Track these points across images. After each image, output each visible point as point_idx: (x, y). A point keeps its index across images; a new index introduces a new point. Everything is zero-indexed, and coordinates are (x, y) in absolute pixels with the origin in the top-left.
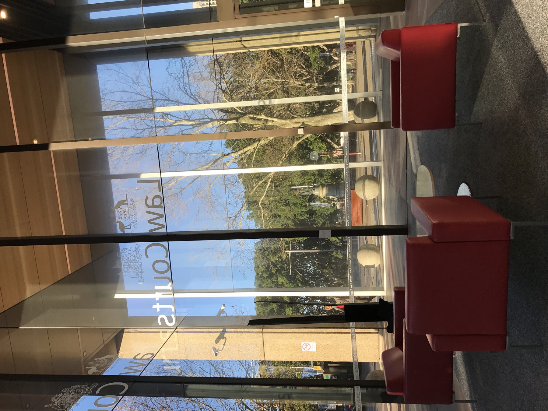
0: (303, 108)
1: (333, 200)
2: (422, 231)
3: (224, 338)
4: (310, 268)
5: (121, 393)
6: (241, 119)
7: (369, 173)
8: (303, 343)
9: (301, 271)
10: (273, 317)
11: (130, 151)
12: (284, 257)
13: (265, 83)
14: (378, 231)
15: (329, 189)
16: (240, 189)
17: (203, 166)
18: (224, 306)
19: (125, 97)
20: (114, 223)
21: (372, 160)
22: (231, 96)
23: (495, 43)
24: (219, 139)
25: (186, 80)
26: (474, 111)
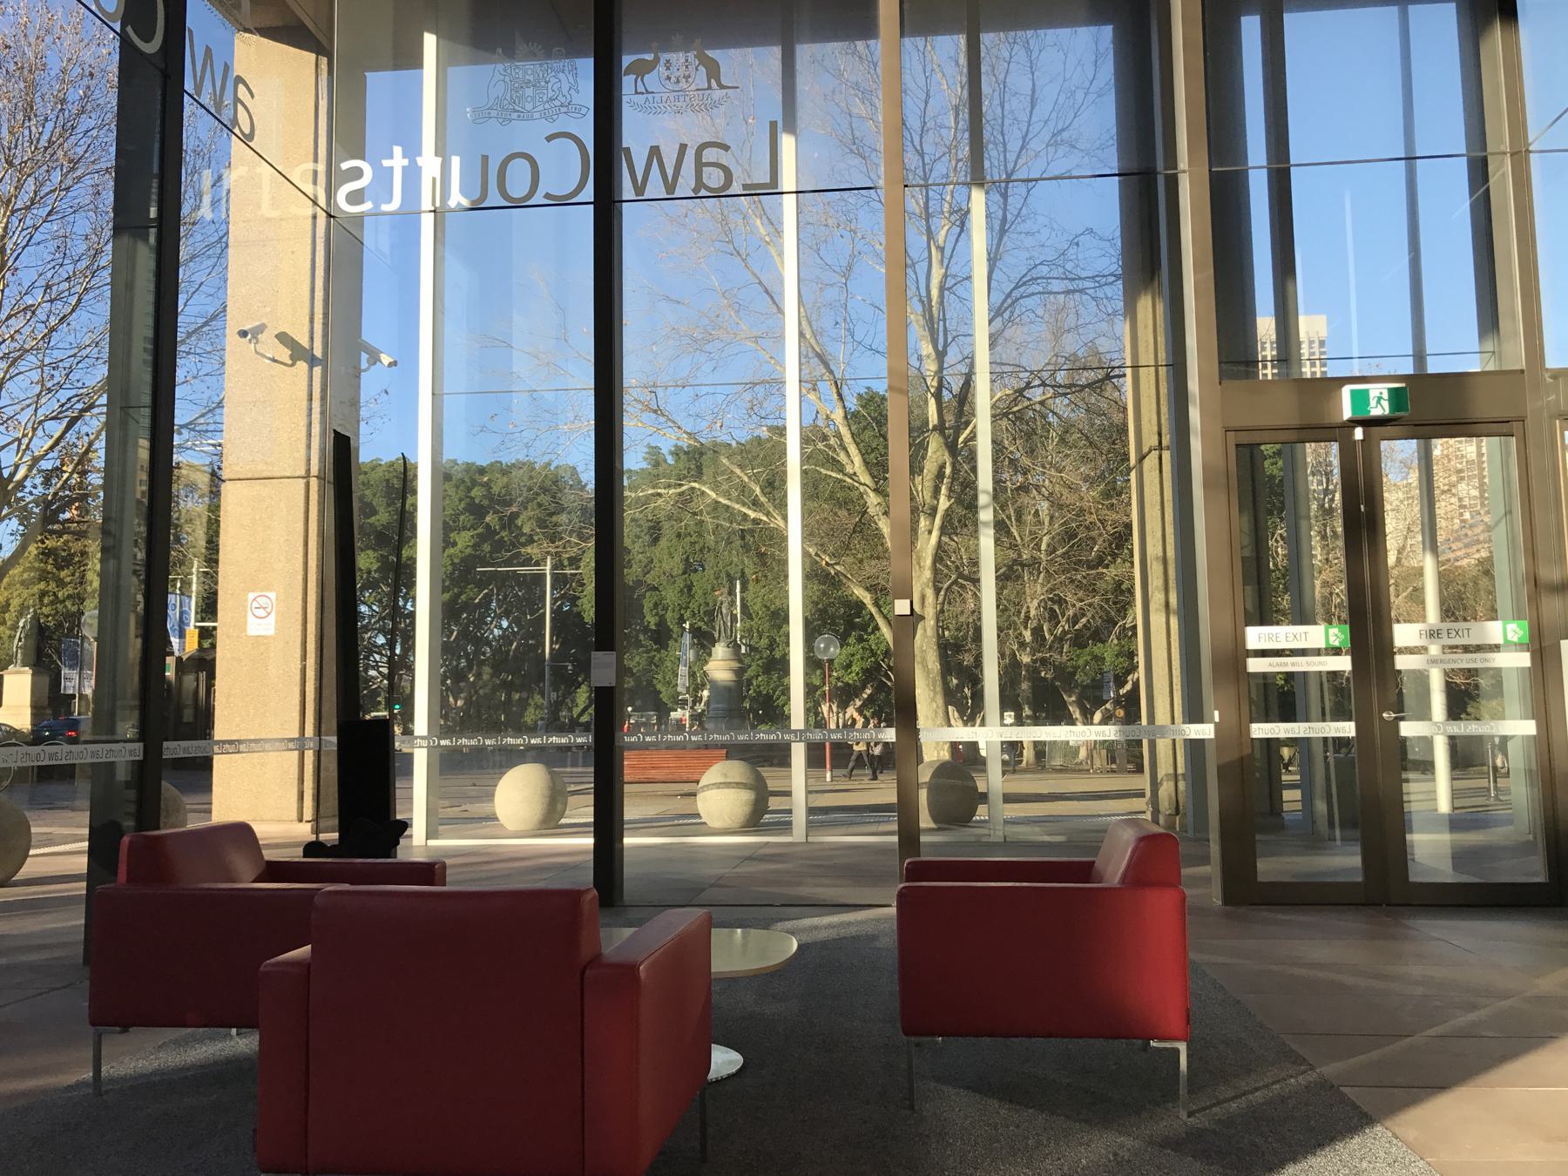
0: (962, 619)
1: (697, 700)
2: (616, 939)
3: (294, 359)
4: (499, 627)
5: (129, 29)
6: (941, 440)
7: (774, 803)
8: (273, 595)
9: (487, 600)
10: (355, 511)
11: (859, 108)
12: (532, 550)
13: (1037, 513)
14: (608, 825)
15: (728, 689)
16: (737, 429)
17: (810, 323)
18: (390, 365)
19: (1017, 105)
20: (655, 44)
21: (811, 811)
22: (1006, 415)
23: (1128, 1142)
24: (891, 371)
25: (1056, 286)
26: (945, 1088)
